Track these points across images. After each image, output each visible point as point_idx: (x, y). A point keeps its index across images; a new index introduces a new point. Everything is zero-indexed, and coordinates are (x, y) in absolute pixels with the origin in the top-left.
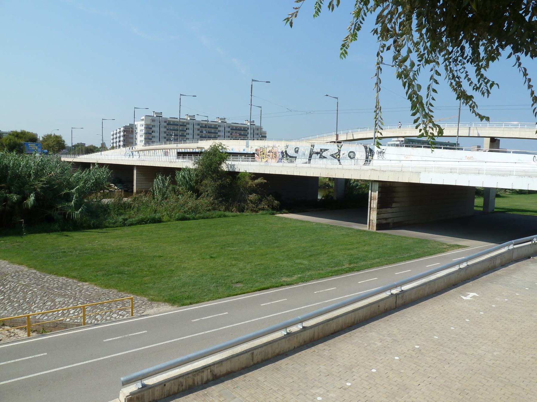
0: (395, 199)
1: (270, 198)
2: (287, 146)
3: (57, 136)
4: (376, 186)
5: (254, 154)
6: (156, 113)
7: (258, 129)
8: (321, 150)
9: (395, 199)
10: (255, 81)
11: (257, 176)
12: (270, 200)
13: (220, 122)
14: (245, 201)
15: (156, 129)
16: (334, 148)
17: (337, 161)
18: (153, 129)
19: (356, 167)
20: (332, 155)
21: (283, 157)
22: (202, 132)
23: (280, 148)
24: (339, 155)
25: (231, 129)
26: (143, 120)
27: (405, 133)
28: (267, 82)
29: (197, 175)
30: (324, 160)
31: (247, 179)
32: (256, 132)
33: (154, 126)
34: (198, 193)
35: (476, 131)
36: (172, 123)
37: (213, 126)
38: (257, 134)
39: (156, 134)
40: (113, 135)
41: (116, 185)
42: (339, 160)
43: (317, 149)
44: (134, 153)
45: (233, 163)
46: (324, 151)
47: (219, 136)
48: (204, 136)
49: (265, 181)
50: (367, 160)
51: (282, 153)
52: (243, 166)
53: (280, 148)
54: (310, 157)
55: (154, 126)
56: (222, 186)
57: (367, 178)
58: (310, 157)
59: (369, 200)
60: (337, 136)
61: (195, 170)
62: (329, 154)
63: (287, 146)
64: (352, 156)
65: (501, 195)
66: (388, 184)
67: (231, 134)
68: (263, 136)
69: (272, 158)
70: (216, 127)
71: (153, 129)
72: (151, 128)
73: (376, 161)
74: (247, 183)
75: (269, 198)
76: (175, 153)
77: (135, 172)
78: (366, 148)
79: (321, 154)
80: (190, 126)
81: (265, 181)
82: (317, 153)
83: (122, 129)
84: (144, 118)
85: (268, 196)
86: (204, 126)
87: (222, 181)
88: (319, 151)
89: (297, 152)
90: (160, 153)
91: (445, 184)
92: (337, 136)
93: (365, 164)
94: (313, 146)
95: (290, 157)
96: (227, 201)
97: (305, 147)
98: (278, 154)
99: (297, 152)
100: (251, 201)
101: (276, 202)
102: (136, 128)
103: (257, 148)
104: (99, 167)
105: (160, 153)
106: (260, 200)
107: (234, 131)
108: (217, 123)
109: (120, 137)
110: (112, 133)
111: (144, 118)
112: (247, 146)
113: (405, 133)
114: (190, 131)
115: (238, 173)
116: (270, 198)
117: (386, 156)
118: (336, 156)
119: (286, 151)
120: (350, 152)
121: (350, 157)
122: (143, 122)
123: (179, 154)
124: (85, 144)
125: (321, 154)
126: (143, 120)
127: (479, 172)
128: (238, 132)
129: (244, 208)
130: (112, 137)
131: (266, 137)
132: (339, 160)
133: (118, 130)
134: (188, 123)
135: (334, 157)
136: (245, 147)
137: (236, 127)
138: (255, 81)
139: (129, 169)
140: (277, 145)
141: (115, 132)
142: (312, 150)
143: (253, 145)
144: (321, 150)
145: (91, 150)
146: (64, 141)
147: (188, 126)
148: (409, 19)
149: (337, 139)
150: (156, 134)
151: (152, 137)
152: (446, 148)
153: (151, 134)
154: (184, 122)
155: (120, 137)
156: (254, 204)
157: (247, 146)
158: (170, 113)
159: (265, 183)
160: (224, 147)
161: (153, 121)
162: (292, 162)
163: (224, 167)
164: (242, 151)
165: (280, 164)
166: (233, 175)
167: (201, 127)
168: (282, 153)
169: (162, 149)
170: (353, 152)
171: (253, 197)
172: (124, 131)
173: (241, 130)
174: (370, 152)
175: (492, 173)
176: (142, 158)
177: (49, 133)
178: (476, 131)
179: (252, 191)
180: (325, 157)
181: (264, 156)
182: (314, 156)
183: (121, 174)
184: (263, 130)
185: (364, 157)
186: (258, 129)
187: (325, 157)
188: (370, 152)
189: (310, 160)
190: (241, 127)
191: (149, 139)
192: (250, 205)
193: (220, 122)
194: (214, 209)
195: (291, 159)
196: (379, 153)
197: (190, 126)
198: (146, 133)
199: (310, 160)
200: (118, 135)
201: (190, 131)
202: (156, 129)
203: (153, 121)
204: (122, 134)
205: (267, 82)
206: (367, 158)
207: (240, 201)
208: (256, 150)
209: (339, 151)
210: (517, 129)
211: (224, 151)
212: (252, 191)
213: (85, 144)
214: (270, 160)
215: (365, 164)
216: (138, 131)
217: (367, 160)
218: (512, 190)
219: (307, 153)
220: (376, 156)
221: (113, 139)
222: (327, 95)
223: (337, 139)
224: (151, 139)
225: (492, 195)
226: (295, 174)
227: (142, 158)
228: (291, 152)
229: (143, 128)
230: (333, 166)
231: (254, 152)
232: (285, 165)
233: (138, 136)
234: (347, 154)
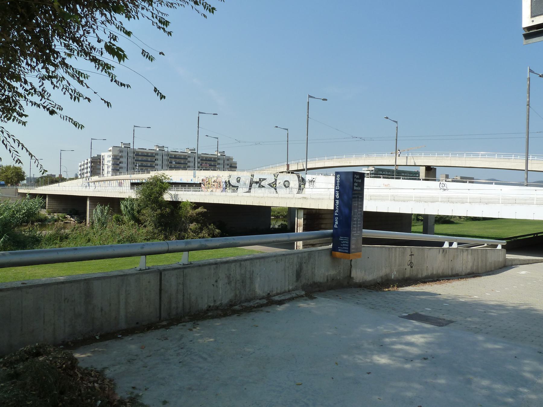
0: (323, 226)
1: (212, 227)
2: (230, 176)
3: (16, 167)
4: (301, 213)
5: (200, 184)
6: (124, 144)
7: (228, 160)
8: (260, 179)
9: (323, 226)
10: (202, 113)
11: (197, 205)
12: (212, 229)
13: (189, 152)
14: (186, 230)
15: (124, 160)
16: (271, 179)
17: (273, 190)
18: (121, 160)
19: (290, 196)
20: (269, 185)
21: (226, 186)
22: (171, 163)
23: (224, 178)
24: (276, 184)
25: (201, 160)
26: (110, 151)
27: (350, 163)
28: (214, 114)
29: (139, 205)
30: (263, 189)
31: (189, 208)
32: (226, 162)
33: (121, 157)
34: (138, 221)
35: (412, 161)
36: (140, 154)
37: (182, 157)
38: (228, 165)
39: (124, 165)
40: (81, 166)
41: (72, 217)
42: (276, 189)
43: (256, 179)
44: (90, 184)
45: (177, 193)
46: (263, 180)
47: (189, 167)
48: (173, 166)
49: (205, 210)
50: (300, 189)
51: (226, 182)
52: (187, 196)
53: (224, 178)
54: (251, 186)
55: (121, 157)
56: (162, 216)
57: (292, 206)
58: (251, 186)
59: (296, 227)
60: (288, 166)
61: (137, 200)
62: (267, 183)
63: (230, 176)
64: (286, 185)
65: (455, 222)
66: (314, 211)
67: (201, 165)
68: (232, 167)
69: (217, 188)
70: (185, 158)
71: (121, 160)
72: (119, 159)
73: (308, 190)
74: (188, 212)
75: (210, 227)
76: (128, 183)
77: (88, 202)
78: (299, 177)
79: (259, 183)
80: (159, 157)
81: (205, 210)
82: (257, 183)
83: (89, 160)
84: (111, 148)
85: (210, 225)
86: (173, 156)
87: (161, 211)
88: (258, 180)
89: (238, 181)
90: (115, 183)
91: (401, 212)
92: (288, 166)
93: (298, 193)
94: (253, 176)
95: (233, 186)
96: (165, 230)
97: (245, 176)
98: (222, 184)
99: (238, 181)
100: (191, 229)
101: (217, 231)
102: (103, 159)
103: (203, 178)
104: (31, 198)
105: (115, 183)
106: (201, 229)
107: (204, 162)
108: (186, 154)
109: (87, 168)
110: (80, 164)
111: (111, 148)
112: (195, 176)
113: (350, 163)
114: (159, 162)
115: (180, 202)
116: (212, 227)
117: (316, 185)
118: (273, 185)
119: (229, 181)
120: (285, 181)
121: (285, 185)
122: (111, 153)
123: (133, 184)
124: (55, 175)
125: (259, 183)
126: (110, 151)
127: (394, 199)
128: (209, 162)
129: (184, 237)
130: (80, 168)
131: (236, 167)
132: (276, 189)
133: (86, 161)
134: (157, 154)
135: (271, 186)
136: (192, 177)
137: (206, 158)
138: (202, 113)
139: (82, 200)
140: (221, 176)
141: (83, 163)
142: (252, 179)
143: (223, 175)
144: (260, 179)
145: (53, 180)
146: (24, 173)
147: (157, 157)
148: (9, 85)
149: (288, 168)
150: (124, 165)
151: (120, 168)
152: (405, 179)
153: (118, 165)
154: (152, 153)
155: (87, 168)
156: (195, 233)
157: (195, 176)
158: (145, 143)
159: (205, 212)
160: (167, 177)
161: (121, 151)
162: (234, 191)
163: (167, 197)
164: (190, 182)
165: (224, 193)
166: (176, 204)
167: (170, 158)
168: (226, 182)
169: (117, 180)
170: (287, 181)
171: (193, 226)
172: (92, 162)
173: (211, 161)
174: (302, 181)
175: (419, 200)
176: (98, 188)
177: (8, 165)
178: (412, 161)
179: (192, 220)
180: (263, 187)
181: (210, 185)
182: (254, 185)
183: (75, 205)
184: (234, 160)
185: (297, 186)
186: (228, 160)
187: (263, 187)
188: (302, 181)
189: (250, 189)
190: (211, 158)
191: (117, 168)
192: (191, 234)
193: (189, 152)
194: (153, 238)
195: (233, 188)
197: (159, 157)
198: (113, 164)
199: (250, 189)
200: (86, 166)
201: (159, 162)
202: (124, 160)
203: (121, 151)
204: (89, 165)
205: (214, 114)
206: (300, 186)
207: (181, 230)
208: (203, 180)
209: (276, 180)
210: (448, 158)
211: (167, 181)
212: (192, 220)
213: (55, 175)
214: (214, 190)
215: (298, 193)
216: (105, 162)
217: (300, 189)
218: (467, 217)
219: (248, 183)
220: (307, 184)
221: (80, 170)
222: (277, 127)
223: (288, 168)
224: (118, 170)
225: (431, 221)
226: (231, 203)
227: (98, 188)
228: (234, 182)
229: (110, 159)
230: (270, 195)
231: (201, 182)
232: (227, 194)
233: (105, 167)
234: (282, 183)
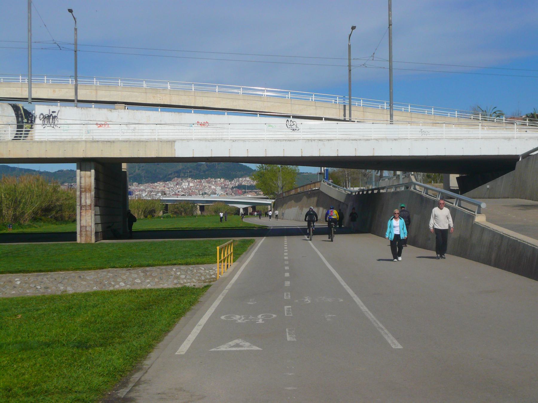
73: (40, 132)
196: (45, 118)
